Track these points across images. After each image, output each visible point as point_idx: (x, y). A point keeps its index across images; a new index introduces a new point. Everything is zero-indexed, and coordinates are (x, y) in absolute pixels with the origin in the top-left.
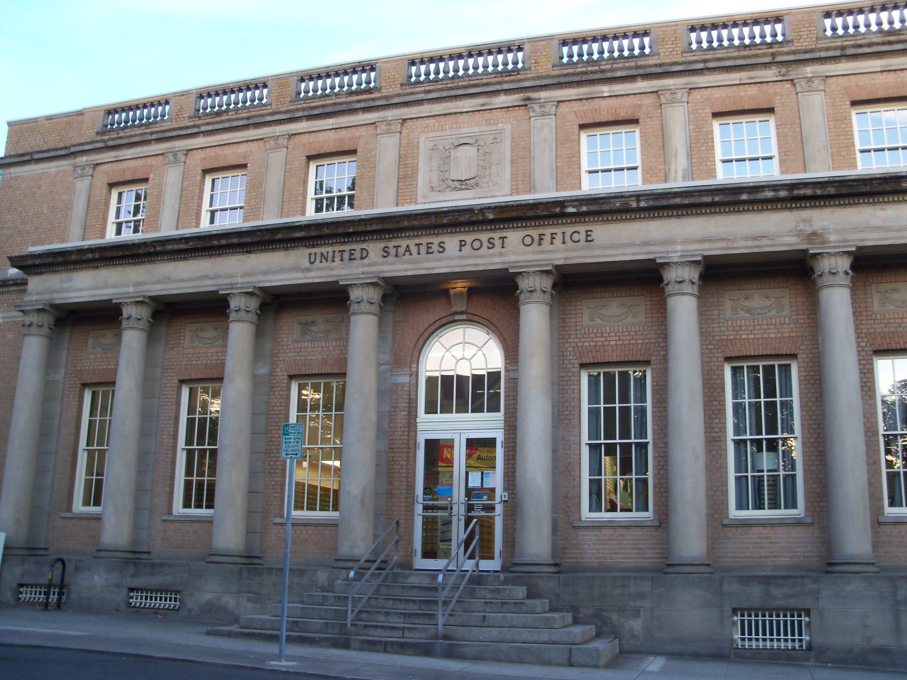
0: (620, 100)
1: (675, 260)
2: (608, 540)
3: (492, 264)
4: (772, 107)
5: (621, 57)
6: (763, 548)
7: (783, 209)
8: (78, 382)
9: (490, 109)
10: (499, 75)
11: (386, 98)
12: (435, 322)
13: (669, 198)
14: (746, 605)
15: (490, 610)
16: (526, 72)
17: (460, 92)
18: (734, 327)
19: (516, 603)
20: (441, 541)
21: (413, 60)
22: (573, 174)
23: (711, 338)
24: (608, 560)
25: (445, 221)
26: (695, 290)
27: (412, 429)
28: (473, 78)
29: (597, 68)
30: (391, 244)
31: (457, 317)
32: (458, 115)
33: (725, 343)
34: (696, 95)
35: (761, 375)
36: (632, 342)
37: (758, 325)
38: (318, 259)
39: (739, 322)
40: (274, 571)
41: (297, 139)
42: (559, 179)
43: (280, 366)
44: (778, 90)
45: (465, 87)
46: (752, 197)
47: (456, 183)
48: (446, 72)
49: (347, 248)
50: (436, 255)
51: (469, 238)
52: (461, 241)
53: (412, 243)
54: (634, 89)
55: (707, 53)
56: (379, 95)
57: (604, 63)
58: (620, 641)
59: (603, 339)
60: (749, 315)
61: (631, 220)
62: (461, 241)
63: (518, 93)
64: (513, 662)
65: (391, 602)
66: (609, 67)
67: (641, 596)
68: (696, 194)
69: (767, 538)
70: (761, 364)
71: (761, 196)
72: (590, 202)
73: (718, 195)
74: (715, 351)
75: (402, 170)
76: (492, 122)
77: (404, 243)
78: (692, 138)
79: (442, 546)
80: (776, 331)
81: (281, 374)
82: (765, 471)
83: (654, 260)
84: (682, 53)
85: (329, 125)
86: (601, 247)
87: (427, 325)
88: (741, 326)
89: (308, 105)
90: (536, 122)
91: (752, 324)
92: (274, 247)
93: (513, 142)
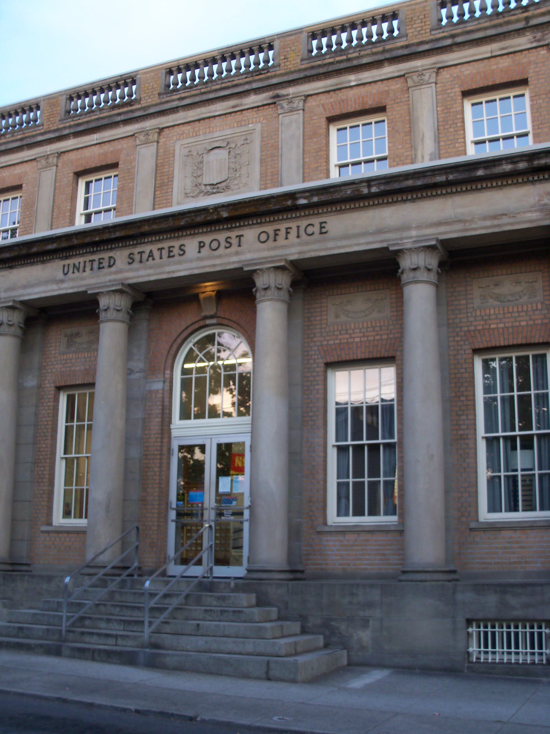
0: (368, 88)
1: (409, 246)
2: (352, 546)
3: (229, 263)
4: (525, 77)
5: (369, 43)
6: (514, 553)
7: (524, 183)
8: (321, 361)
9: (242, 111)
10: (249, 75)
11: (144, 109)
12: (187, 328)
13: (400, 181)
14: (480, 616)
15: (210, 618)
16: (275, 69)
17: (211, 96)
18: (482, 316)
19: (234, 612)
20: (234, 548)
21: (170, 69)
22: (320, 168)
23: (459, 329)
24: (352, 567)
25: (182, 223)
26: (433, 277)
27: (166, 435)
28: (225, 81)
29: (344, 57)
30: (136, 250)
31: (208, 322)
32: (211, 119)
33: (473, 334)
34: (445, 75)
35: (514, 365)
36: (378, 337)
37: (509, 313)
38: (71, 270)
39: (487, 312)
40: (26, 578)
41: (65, 157)
42: (306, 175)
43: (49, 378)
44: (532, 59)
45: (216, 90)
46: (488, 172)
47: (208, 187)
48: (201, 77)
49: (96, 257)
50: (177, 258)
51: (207, 239)
52: (200, 242)
53: (154, 248)
54: (381, 75)
55: (457, 27)
56: (139, 106)
57: (351, 51)
58: (348, 652)
59: (348, 336)
60: (499, 303)
61: (364, 208)
62: (200, 242)
63: (267, 91)
64: (211, 673)
65: (118, 609)
66: (356, 54)
67: (370, 605)
68: (429, 174)
69: (518, 542)
70: (514, 355)
71: (498, 170)
72: (322, 192)
73: (452, 173)
74: (462, 343)
75: (158, 178)
76: (243, 123)
77: (147, 249)
78: (440, 120)
79: (234, 553)
80: (527, 318)
81: (50, 387)
82: (519, 470)
83: (386, 249)
84: (431, 31)
85: (93, 140)
86: (334, 239)
87: (179, 331)
88: (490, 315)
89: (76, 122)
90: (285, 119)
91: (502, 312)
92: (32, 260)
93: (262, 141)
